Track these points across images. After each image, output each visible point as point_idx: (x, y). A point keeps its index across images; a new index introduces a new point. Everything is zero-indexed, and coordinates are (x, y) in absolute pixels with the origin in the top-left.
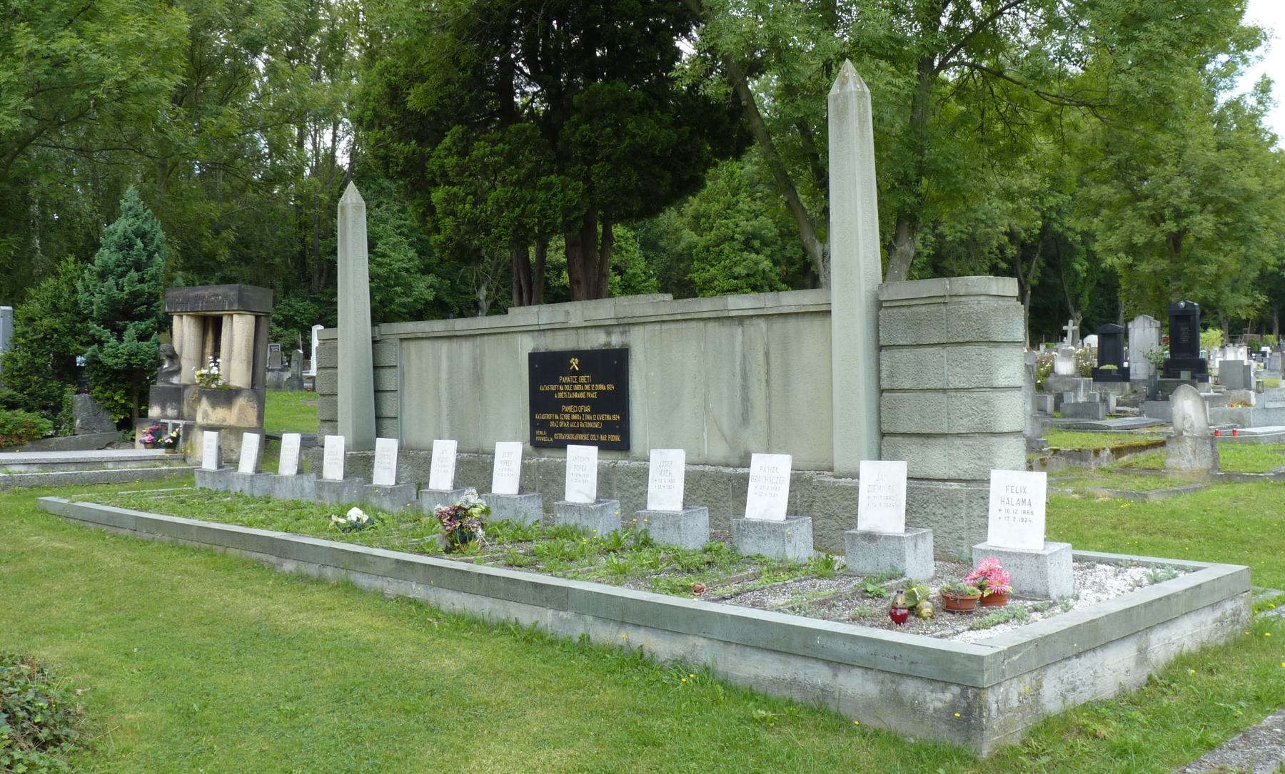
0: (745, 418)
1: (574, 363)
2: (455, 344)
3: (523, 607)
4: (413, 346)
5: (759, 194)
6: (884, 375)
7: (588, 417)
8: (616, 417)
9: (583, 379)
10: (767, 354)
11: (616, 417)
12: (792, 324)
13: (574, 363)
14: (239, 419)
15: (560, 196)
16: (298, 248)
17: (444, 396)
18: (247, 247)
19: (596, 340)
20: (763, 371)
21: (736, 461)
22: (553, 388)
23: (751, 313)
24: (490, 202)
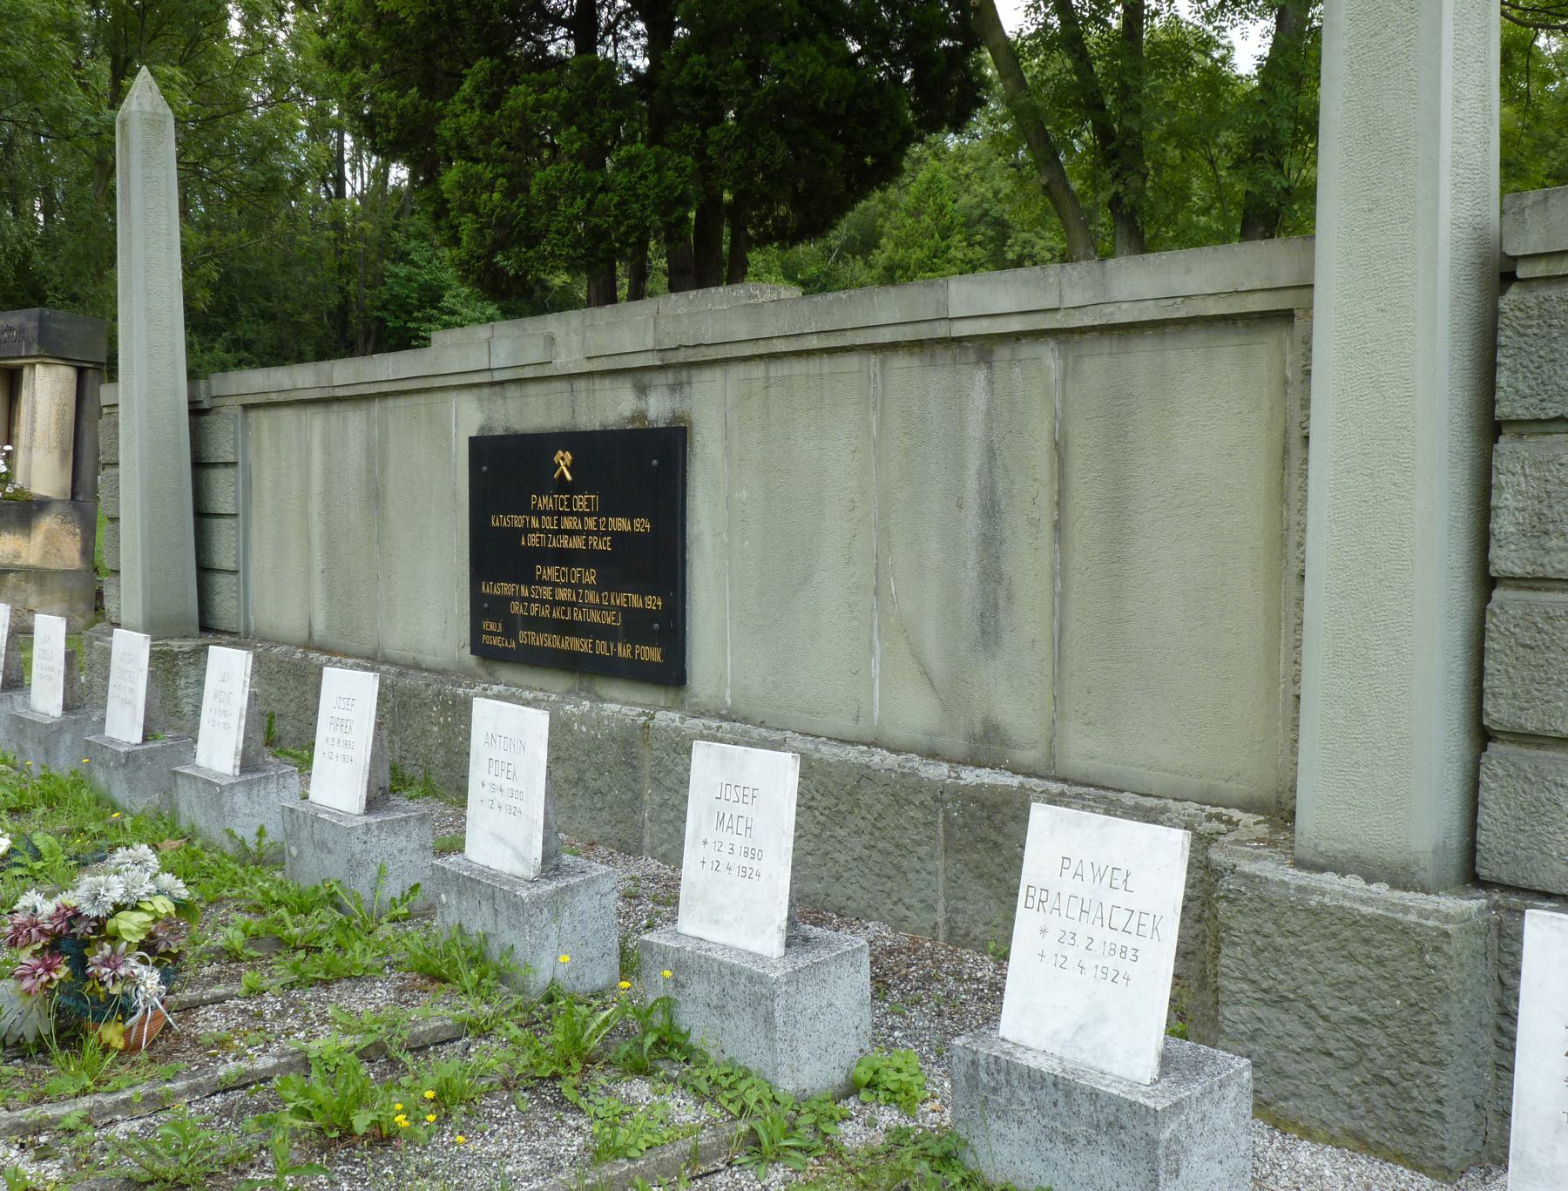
0: (989, 626)
1: (564, 459)
2: (335, 415)
4: (264, 419)
5: (978, 238)
6: (1503, 524)
7: (591, 597)
8: (653, 602)
9: (581, 502)
10: (1060, 448)
11: (653, 602)
12: (1143, 356)
13: (564, 459)
14: (46, 554)
15: (653, 179)
16: (334, 300)
17: (317, 529)
18: (268, 299)
19: (612, 407)
20: (1046, 497)
21: (960, 746)
22: (518, 521)
23: (1015, 325)
24: (534, 191)
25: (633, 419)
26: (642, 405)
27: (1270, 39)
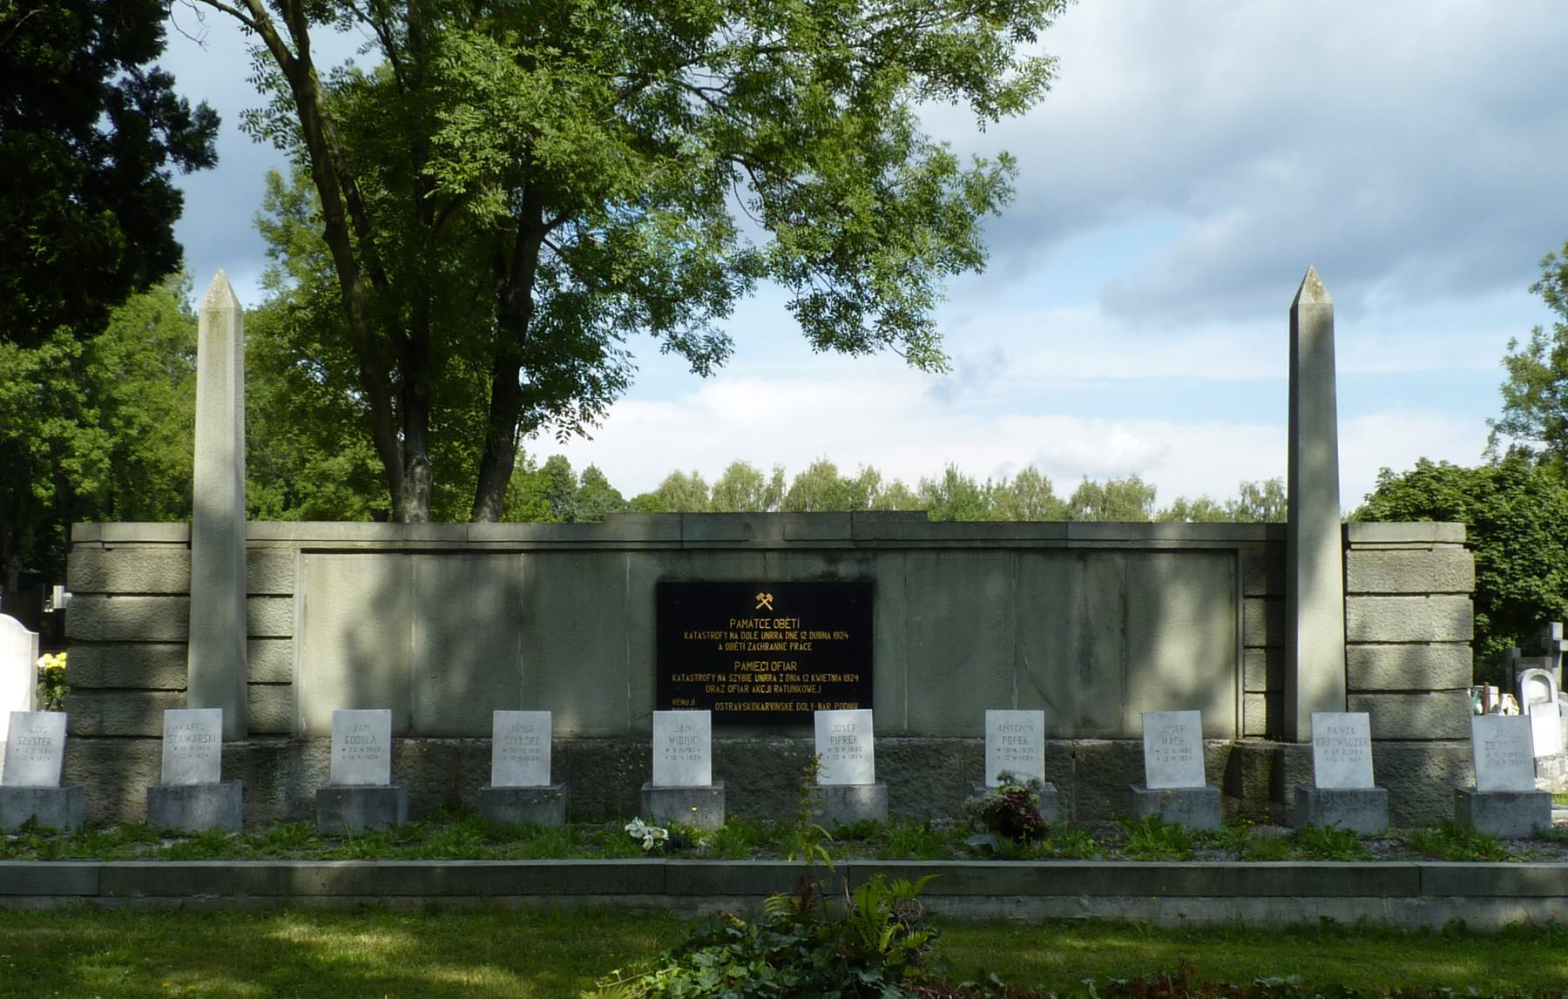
1: (765, 600)
3: (1331, 901)
7: (792, 678)
9: (782, 623)
25: (823, 576)
26: (833, 568)
27: (1010, 516)
